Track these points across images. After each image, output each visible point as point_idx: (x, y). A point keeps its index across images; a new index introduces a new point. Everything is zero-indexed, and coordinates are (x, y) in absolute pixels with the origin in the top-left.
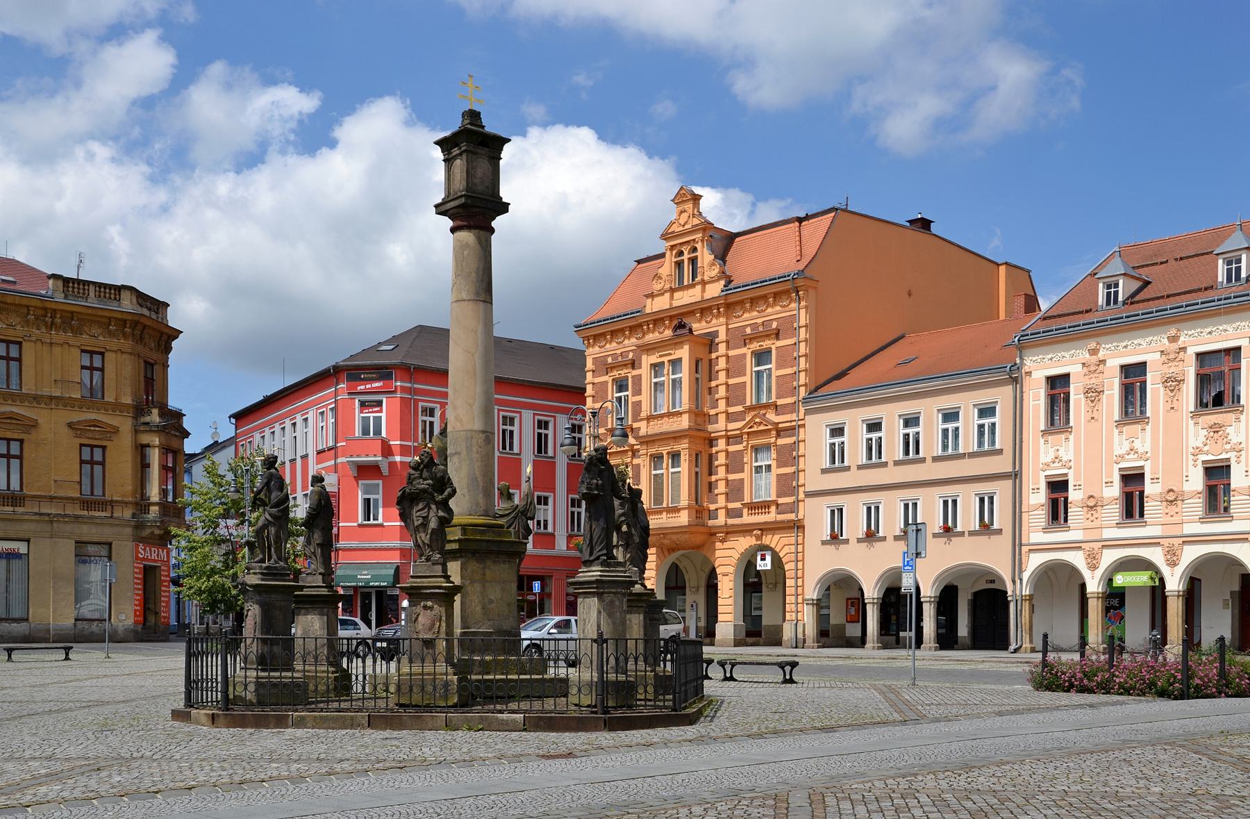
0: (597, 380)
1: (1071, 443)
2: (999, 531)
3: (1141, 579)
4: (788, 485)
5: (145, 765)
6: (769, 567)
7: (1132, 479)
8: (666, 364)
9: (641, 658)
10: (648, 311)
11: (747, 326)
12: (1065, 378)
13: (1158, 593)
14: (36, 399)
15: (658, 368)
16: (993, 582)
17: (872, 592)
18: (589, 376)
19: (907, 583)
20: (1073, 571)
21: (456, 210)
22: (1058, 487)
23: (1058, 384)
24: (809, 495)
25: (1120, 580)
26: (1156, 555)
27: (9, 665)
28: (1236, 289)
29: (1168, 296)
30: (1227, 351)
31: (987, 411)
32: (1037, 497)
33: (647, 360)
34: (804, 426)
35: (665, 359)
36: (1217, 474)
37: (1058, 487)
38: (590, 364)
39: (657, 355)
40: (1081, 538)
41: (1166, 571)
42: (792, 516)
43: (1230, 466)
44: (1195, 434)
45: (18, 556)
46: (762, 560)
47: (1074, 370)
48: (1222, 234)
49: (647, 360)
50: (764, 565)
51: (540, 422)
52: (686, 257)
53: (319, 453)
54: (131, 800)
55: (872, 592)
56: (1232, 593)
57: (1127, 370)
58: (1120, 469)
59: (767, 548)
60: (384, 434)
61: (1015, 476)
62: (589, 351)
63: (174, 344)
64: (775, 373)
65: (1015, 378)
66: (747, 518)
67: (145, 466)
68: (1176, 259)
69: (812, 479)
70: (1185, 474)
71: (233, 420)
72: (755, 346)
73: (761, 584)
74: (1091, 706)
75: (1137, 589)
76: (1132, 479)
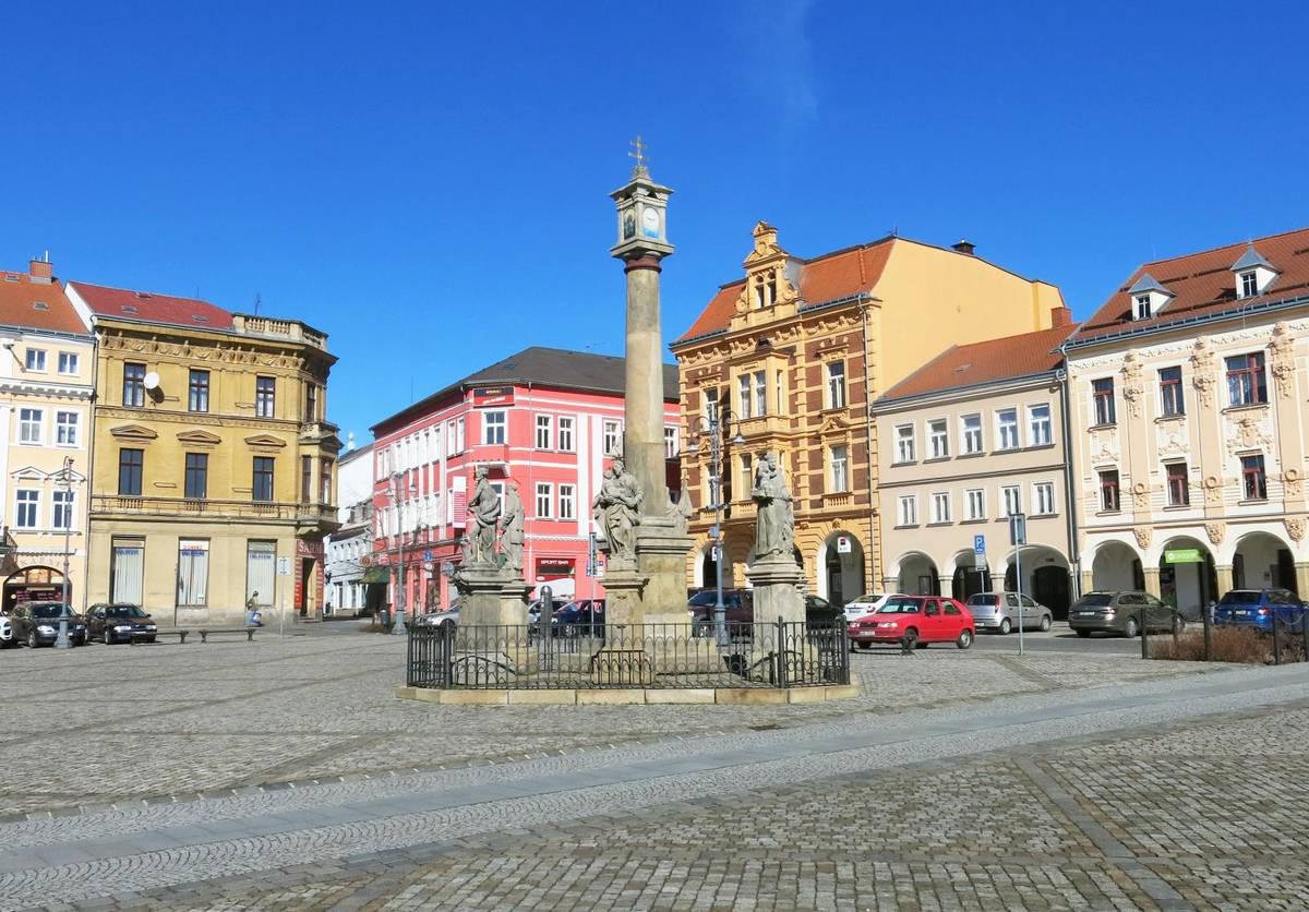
0: (688, 391)
1: (1117, 437)
2: (1056, 516)
3: (1192, 556)
4: (863, 479)
5: (923, 828)
6: (849, 550)
7: (1178, 471)
8: (752, 375)
9: (806, 640)
10: (731, 330)
11: (821, 341)
12: (1109, 380)
13: (1206, 568)
14: (222, 419)
15: (745, 379)
16: (1052, 560)
17: (947, 571)
18: (683, 387)
19: (980, 562)
20: (1125, 549)
21: (628, 254)
22: (1110, 477)
23: (1103, 387)
24: (881, 487)
25: (1172, 557)
26: (1200, 534)
27: (251, 644)
28: (1252, 301)
29: (1195, 307)
30: (1251, 355)
31: (1041, 411)
32: (1089, 488)
33: (735, 371)
34: (875, 427)
35: (751, 371)
36: (1253, 465)
37: (1110, 477)
38: (683, 378)
39: (743, 367)
40: (1131, 521)
41: (1212, 548)
42: (867, 506)
43: (1262, 456)
44: (1228, 429)
45: (201, 552)
46: (842, 544)
47: (1116, 374)
48: (1239, 249)
49: (735, 371)
50: (845, 548)
51: (562, 421)
52: (767, 280)
53: (448, 459)
54: (448, 768)
55: (947, 571)
56: (1272, 567)
57: (1164, 372)
58: (1163, 461)
59: (845, 534)
60: (506, 441)
61: (1067, 468)
62: (681, 366)
63: (331, 369)
64: (848, 382)
65: (1062, 387)
66: (829, 507)
67: (307, 474)
68: (1195, 275)
69: (882, 472)
70: (1222, 463)
71: (373, 432)
72: (829, 358)
73: (839, 565)
74: (1201, 672)
75: (1185, 566)
76: (1178, 471)
